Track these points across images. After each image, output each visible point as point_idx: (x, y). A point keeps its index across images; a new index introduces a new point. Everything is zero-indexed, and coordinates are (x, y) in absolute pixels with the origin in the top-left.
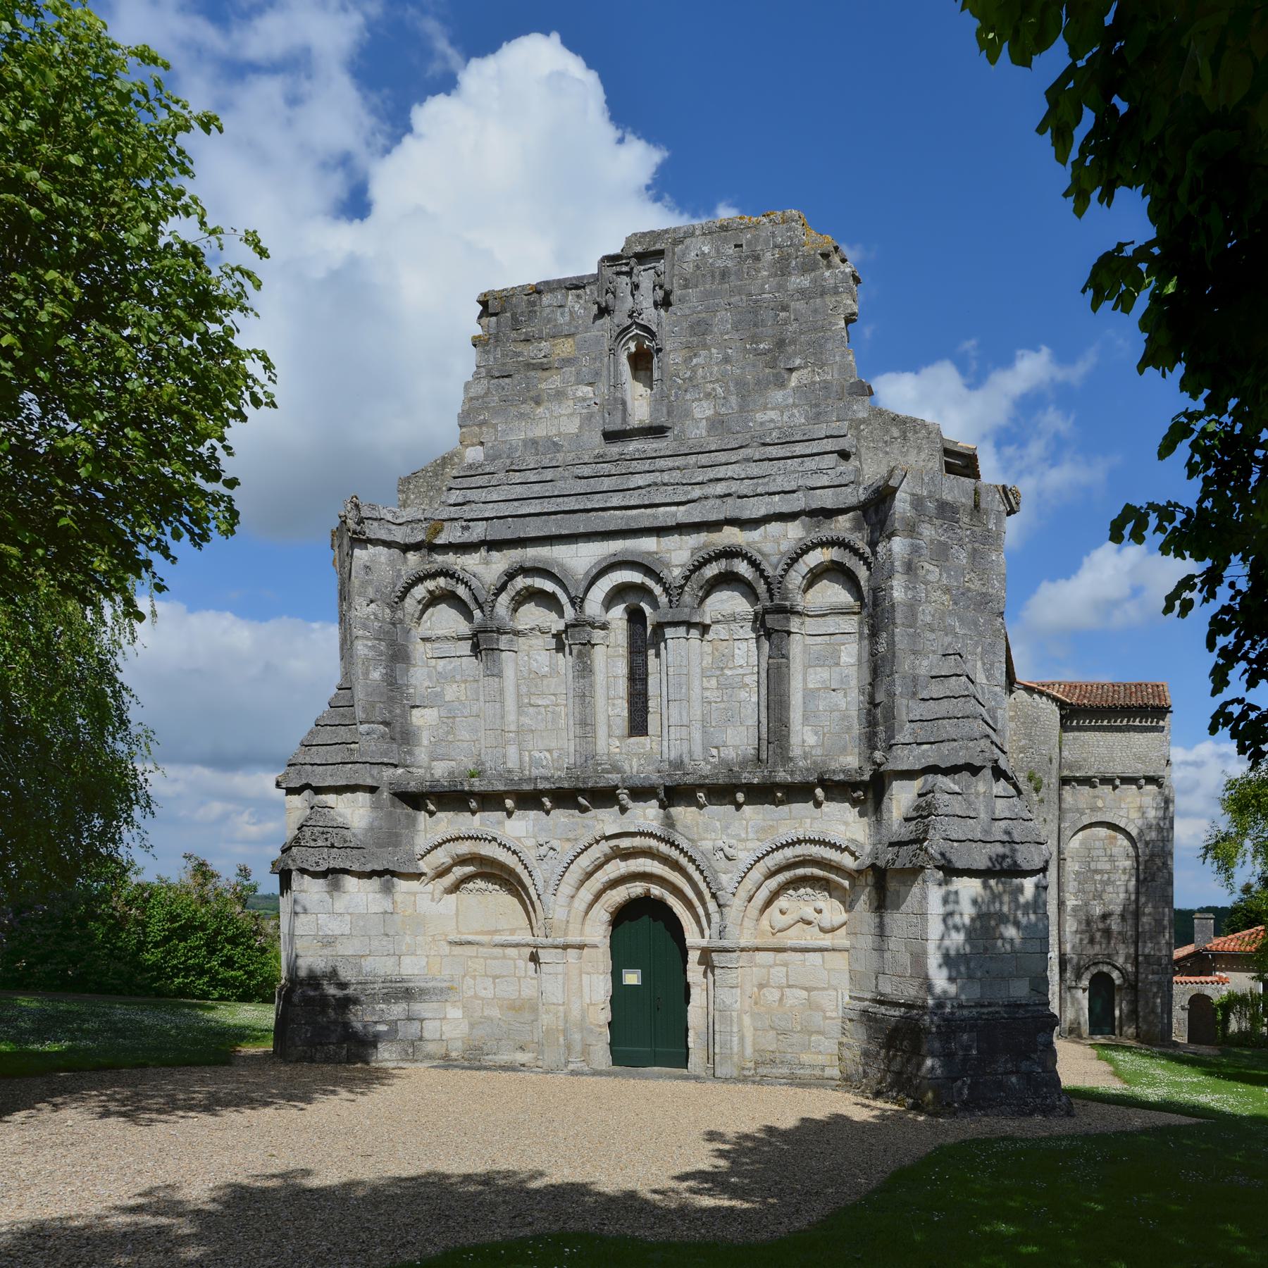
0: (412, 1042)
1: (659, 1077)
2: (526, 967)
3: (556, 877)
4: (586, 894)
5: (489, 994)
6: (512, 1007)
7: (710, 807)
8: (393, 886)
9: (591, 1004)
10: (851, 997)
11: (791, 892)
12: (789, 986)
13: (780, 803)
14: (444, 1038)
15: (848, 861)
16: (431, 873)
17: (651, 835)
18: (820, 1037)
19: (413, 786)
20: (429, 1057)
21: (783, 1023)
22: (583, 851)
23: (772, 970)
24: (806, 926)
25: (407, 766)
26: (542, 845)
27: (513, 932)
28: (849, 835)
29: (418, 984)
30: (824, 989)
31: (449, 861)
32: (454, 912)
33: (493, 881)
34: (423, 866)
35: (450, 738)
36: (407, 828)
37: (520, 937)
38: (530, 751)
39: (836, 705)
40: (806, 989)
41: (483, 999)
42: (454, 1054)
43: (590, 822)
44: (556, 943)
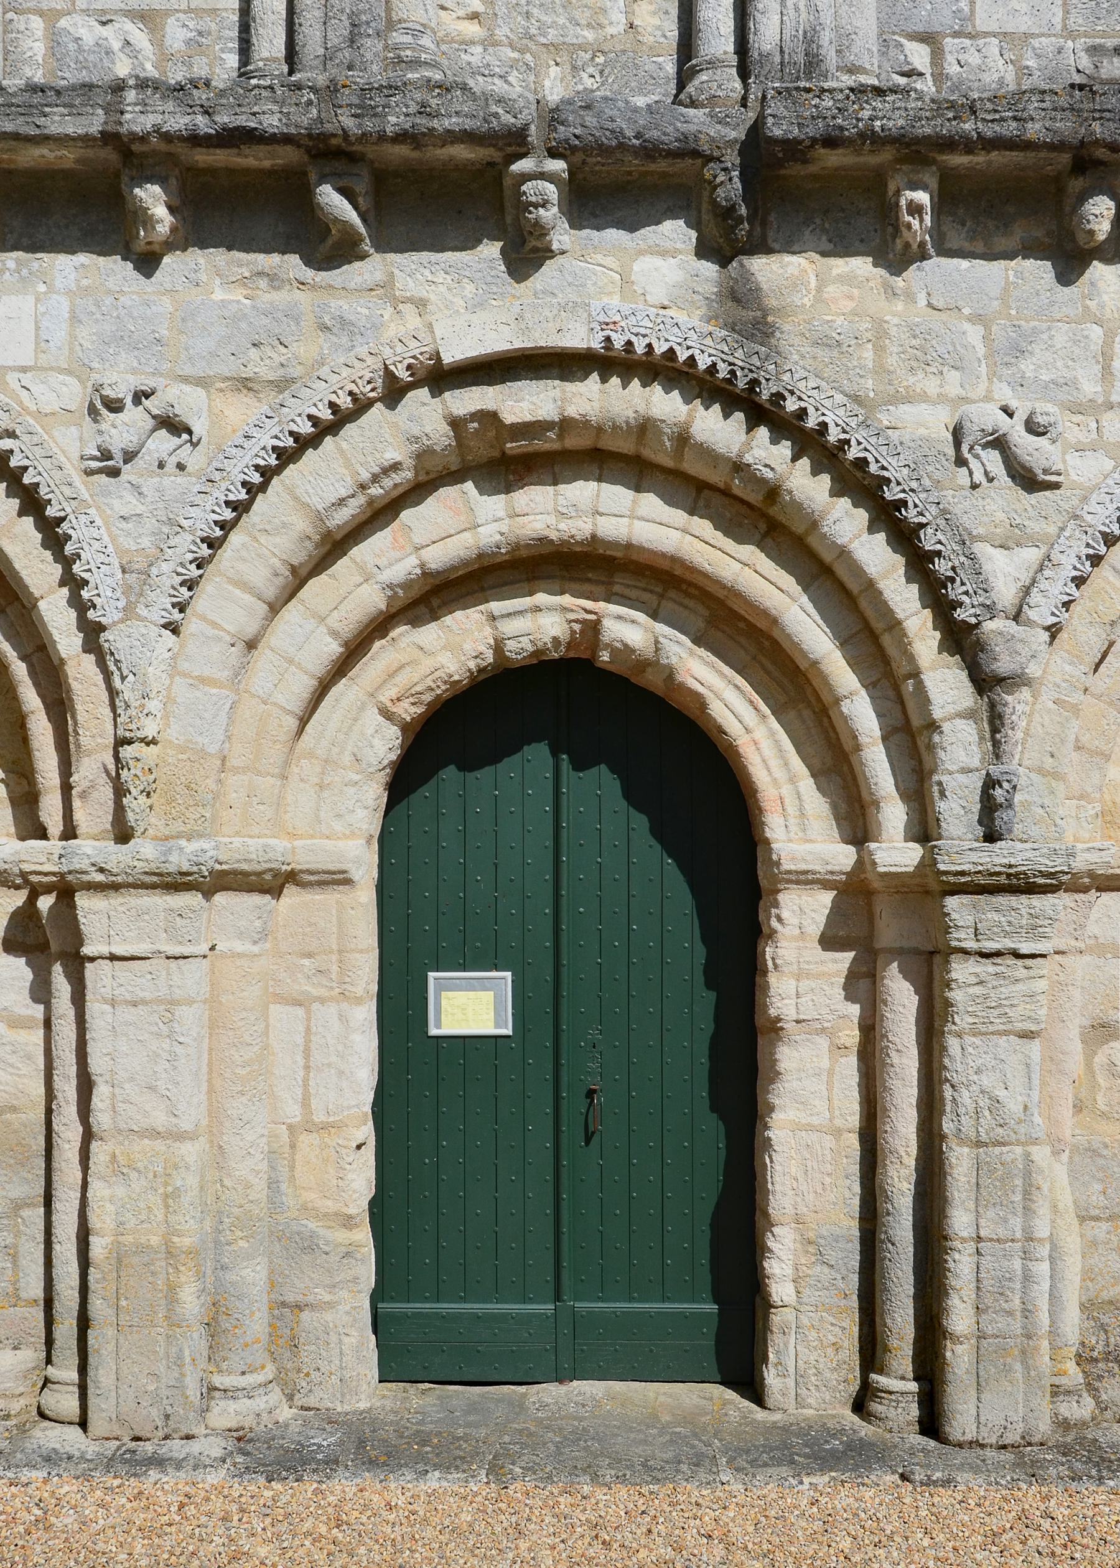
3: (185, 546)
9: (310, 1126)
26: (114, 406)
38: (50, 16)
43: (357, 309)
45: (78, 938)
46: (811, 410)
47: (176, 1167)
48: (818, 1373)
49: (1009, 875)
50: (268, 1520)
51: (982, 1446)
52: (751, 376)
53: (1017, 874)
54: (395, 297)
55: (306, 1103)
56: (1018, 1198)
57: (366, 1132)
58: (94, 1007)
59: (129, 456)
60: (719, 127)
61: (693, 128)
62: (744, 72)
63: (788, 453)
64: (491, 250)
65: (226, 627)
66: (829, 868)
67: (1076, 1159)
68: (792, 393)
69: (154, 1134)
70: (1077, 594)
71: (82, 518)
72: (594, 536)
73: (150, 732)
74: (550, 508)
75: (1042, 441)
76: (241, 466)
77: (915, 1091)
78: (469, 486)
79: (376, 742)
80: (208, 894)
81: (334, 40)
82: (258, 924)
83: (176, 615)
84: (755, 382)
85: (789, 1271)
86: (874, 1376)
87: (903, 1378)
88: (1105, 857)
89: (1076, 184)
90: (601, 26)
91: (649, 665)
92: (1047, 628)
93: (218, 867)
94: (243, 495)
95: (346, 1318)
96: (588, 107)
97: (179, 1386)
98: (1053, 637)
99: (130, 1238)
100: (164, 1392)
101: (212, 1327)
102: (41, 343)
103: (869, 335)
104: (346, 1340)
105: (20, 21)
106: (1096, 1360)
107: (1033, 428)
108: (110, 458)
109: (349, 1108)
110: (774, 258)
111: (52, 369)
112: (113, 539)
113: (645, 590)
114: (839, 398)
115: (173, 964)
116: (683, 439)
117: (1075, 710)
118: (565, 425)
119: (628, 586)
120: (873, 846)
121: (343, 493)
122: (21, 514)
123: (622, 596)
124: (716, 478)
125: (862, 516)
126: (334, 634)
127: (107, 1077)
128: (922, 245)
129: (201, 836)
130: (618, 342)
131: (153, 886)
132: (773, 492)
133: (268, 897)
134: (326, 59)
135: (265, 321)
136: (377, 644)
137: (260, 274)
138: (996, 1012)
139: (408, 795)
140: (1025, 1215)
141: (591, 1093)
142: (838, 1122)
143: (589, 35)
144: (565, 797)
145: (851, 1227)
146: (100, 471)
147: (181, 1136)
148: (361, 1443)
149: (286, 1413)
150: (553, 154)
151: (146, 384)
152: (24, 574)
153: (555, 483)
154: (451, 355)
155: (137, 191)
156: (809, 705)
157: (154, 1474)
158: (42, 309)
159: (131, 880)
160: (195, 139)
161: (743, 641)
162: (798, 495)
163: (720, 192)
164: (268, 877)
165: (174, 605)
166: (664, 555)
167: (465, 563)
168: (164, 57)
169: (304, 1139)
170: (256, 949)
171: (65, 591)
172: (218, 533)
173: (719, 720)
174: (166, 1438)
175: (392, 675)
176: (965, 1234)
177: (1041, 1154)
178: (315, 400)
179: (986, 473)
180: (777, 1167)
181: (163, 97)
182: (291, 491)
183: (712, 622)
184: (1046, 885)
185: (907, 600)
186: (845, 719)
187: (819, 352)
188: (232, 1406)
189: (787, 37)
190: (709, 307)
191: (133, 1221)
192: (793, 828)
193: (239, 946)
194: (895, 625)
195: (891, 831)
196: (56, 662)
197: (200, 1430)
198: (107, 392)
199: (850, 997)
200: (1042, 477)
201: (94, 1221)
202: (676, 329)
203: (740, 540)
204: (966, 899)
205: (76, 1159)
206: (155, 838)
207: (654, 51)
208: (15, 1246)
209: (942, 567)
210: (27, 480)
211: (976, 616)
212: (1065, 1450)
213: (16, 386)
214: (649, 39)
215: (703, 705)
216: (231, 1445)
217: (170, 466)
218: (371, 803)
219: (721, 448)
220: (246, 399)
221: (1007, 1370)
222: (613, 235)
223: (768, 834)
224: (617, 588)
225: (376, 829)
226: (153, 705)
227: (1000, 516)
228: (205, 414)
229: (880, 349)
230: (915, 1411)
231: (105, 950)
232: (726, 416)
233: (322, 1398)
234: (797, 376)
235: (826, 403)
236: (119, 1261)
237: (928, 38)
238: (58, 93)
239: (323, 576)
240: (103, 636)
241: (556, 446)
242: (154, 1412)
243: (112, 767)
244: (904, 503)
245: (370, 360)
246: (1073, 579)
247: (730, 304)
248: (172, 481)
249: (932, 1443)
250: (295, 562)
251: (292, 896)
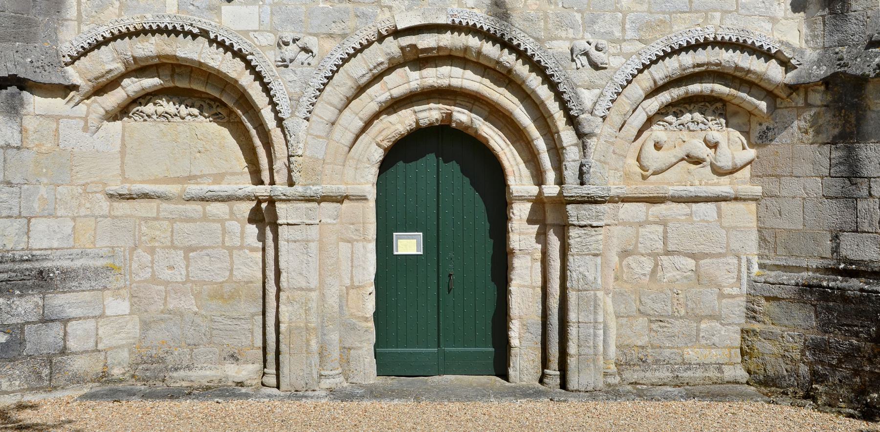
0: (49, 361)
1: (446, 395)
3: (311, 92)
4: (352, 120)
5: (178, 275)
6: (217, 295)
8: (22, 105)
10: (762, 266)
11: (670, 118)
12: (668, 253)
14: (100, 347)
15: (774, 72)
17: (473, 30)
18: (716, 324)
20: (77, 380)
21: (658, 306)
22: (357, 51)
23: (642, 230)
27: (219, 178)
28: (777, 36)
29: (58, 263)
30: (720, 255)
31: (118, 67)
32: (118, 148)
33: (189, 102)
34: (73, 75)
36: (47, 13)
37: (236, 187)
40: (692, 256)
41: (167, 283)
42: (117, 372)
45: (276, 217)
46: (522, 44)
47: (309, 300)
49: (588, 197)
50: (343, 411)
52: (502, 32)
53: (591, 197)
54: (381, 6)
55: (352, 279)
56: (592, 308)
57: (372, 289)
58: (282, 243)
59: (291, 61)
63: (515, 58)
65: (324, 118)
66: (530, 194)
67: (616, 296)
68: (515, 38)
69: (302, 289)
70: (612, 105)
71: (276, 82)
72: (449, 85)
73: (300, 153)
75: (600, 53)
78: (407, 68)
79: (375, 154)
80: (319, 203)
83: (309, 115)
84: (503, 35)
85: (517, 335)
86: (545, 370)
87: (555, 370)
88: (623, 191)
91: (470, 127)
92: (602, 117)
93: (323, 194)
94: (331, 74)
95: (366, 352)
97: (311, 374)
98: (604, 120)
99: (294, 324)
100: (305, 376)
101: (321, 355)
102: (261, 22)
103: (542, 17)
104: (366, 360)
106: (622, 365)
108: (285, 61)
109: (367, 280)
111: (265, 31)
112: (286, 89)
113: (468, 102)
114: (531, 40)
115: (308, 227)
116: (479, 53)
117: (613, 144)
118: (439, 48)
119: (462, 101)
120: (543, 186)
121: (364, 73)
122: (254, 80)
123: (460, 104)
124: (491, 65)
125: (540, 79)
126: (361, 119)
127: (286, 270)
129: (317, 184)
130: (457, 22)
131: (302, 200)
132: (510, 71)
133: (339, 204)
135: (337, 14)
136: (376, 122)
138: (585, 247)
139: (386, 171)
140: (594, 314)
141: (450, 275)
142: (534, 284)
144: (441, 173)
145: (539, 320)
146: (282, 66)
147: (311, 290)
148: (372, 392)
149: (345, 384)
151: (297, 36)
152: (256, 101)
153: (436, 67)
154: (400, 27)
156: (524, 141)
157: (304, 400)
159: (294, 198)
161: (501, 119)
162: (518, 72)
164: (339, 197)
165: (307, 112)
167: (405, 94)
170: (335, 222)
171: (270, 106)
172: (322, 87)
173: (493, 146)
174: (306, 391)
176: (574, 321)
177: (600, 294)
178: (355, 42)
179: (582, 64)
180: (513, 300)
182: (346, 72)
183: (490, 113)
184: (601, 201)
185: (555, 107)
186: (535, 146)
188: (328, 381)
191: (295, 319)
193: (329, 221)
194: (551, 116)
195: (550, 181)
196: (267, 130)
197: (317, 388)
198: (284, 39)
199: (538, 242)
200: (600, 65)
201: (281, 318)
202: (476, 17)
203: (499, 86)
204: (574, 206)
206: (302, 185)
208: (252, 329)
209: (566, 97)
210: (257, 69)
211: (577, 113)
213: (253, 37)
216: (328, 392)
217: (306, 64)
219: (492, 56)
220: (332, 40)
223: (509, 183)
224: (458, 101)
225: (375, 181)
226: (301, 145)
228: (317, 46)
229: (546, 22)
231: (285, 222)
232: (494, 45)
233: (357, 379)
234: (517, 33)
235: (527, 41)
236: (290, 332)
239: (357, 99)
240: (284, 122)
241: (437, 55)
242: (302, 382)
243: (287, 163)
244: (553, 75)
245: (373, 28)
246: (610, 100)
247: (495, 7)
248: (307, 69)
249: (563, 391)
250: (348, 96)
251: (346, 203)
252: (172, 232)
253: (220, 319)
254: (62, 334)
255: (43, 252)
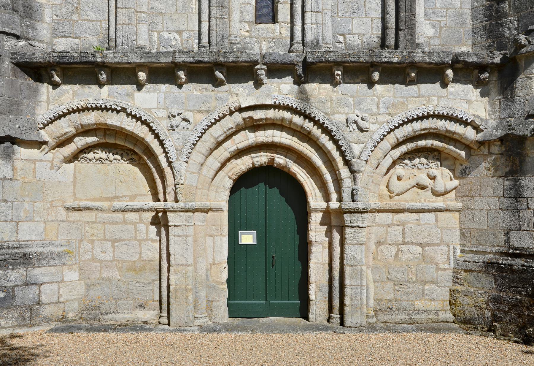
0: (30, 308)
1: (271, 329)
2: (147, 231)
3: (189, 145)
4: (214, 162)
5: (108, 257)
6: (132, 269)
7: (343, 84)
8: (13, 153)
9: (214, 264)
10: (462, 251)
11: (407, 161)
12: (405, 243)
13: (412, 82)
14: (61, 300)
15: (470, 133)
16: (52, 142)
18: (434, 286)
19: (38, 57)
20: (47, 320)
21: (399, 276)
22: (217, 121)
24: (420, 191)
25: (29, 39)
26: (174, 116)
27: (133, 198)
28: (472, 111)
29: (35, 250)
31: (72, 130)
32: (72, 180)
33: (115, 151)
34: (44, 135)
35: (75, 17)
36: (29, 98)
37: (143, 203)
38: (158, 32)
39: (452, 4)
40: (420, 245)
41: (101, 261)
42: (71, 315)
44: (188, 207)
45: (167, 221)
46: (317, 116)
47: (188, 272)
48: (320, 314)
51: (352, 327)
55: (213, 259)
56: (359, 277)
57: (226, 265)
58: (171, 237)
59: (177, 127)
60: (298, 58)
61: (292, 59)
62: (303, 46)
64: (251, 83)
69: (183, 265)
72: (273, 141)
73: (182, 182)
74: (264, 135)
75: (364, 122)
76: (200, 129)
77: (339, 255)
78: (247, 131)
80: (194, 213)
81: (218, 40)
82: (204, 219)
83: (187, 159)
84: (305, 111)
85: (314, 293)
88: (378, 205)
89: (371, 69)
90: (274, 33)
92: (365, 161)
96: (271, 55)
97: (188, 316)
98: (367, 162)
100: (185, 318)
102: (158, 103)
105: (152, 33)
107: (363, 119)
110: (309, 84)
114: (322, 114)
115: (187, 227)
116: (291, 122)
117: (372, 177)
118: (266, 119)
122: (154, 139)
125: (327, 138)
126: (219, 162)
128: (340, 81)
129: (192, 202)
130: (277, 103)
131: (183, 211)
132: (309, 133)
134: (217, 44)
135: (205, 98)
136: (228, 163)
137: (204, 88)
138: (355, 240)
141: (273, 257)
142: (324, 262)
143: (272, 35)
146: (171, 130)
147: (188, 266)
148: (226, 327)
149: (210, 323)
150: (264, 64)
151: (180, 112)
153: (265, 130)
155: (178, 72)
158: (158, 96)
160: (190, 63)
161: (304, 162)
163: (298, 72)
164: (206, 209)
166: (287, 145)
167: (246, 147)
168: (182, 41)
169: (213, 267)
170: (203, 224)
171: (164, 154)
172: (196, 142)
175: (231, 170)
176: (348, 284)
177: (364, 268)
181: (184, 54)
182: (210, 133)
183: (298, 158)
186: (325, 178)
187: (319, 104)
188: (199, 321)
189: (312, 38)
190: (296, 95)
191: (179, 283)
192: (314, 199)
193: (200, 224)
197: (192, 325)
199: (326, 236)
203: (303, 142)
204: (348, 214)
205: (166, 271)
206: (183, 202)
207: (285, 38)
209: (343, 148)
210: (156, 132)
212: (368, 328)
213: (153, 112)
214: (284, 36)
215: (296, 175)
218: (227, 195)
219: (298, 124)
220: (201, 114)
221: (357, 312)
222: (276, 80)
223: (309, 201)
224: (278, 151)
225: (228, 199)
226: (183, 178)
227: (356, 137)
229: (331, 103)
230: (339, 321)
231: (173, 224)
232: (300, 117)
235: (320, 115)
236: (176, 291)
237: (343, 35)
238: (162, 53)
242: (183, 321)
244: (336, 135)
245: (226, 107)
248: (186, 132)
252: (104, 230)
253: (133, 283)
254: (37, 292)
255: (26, 243)
